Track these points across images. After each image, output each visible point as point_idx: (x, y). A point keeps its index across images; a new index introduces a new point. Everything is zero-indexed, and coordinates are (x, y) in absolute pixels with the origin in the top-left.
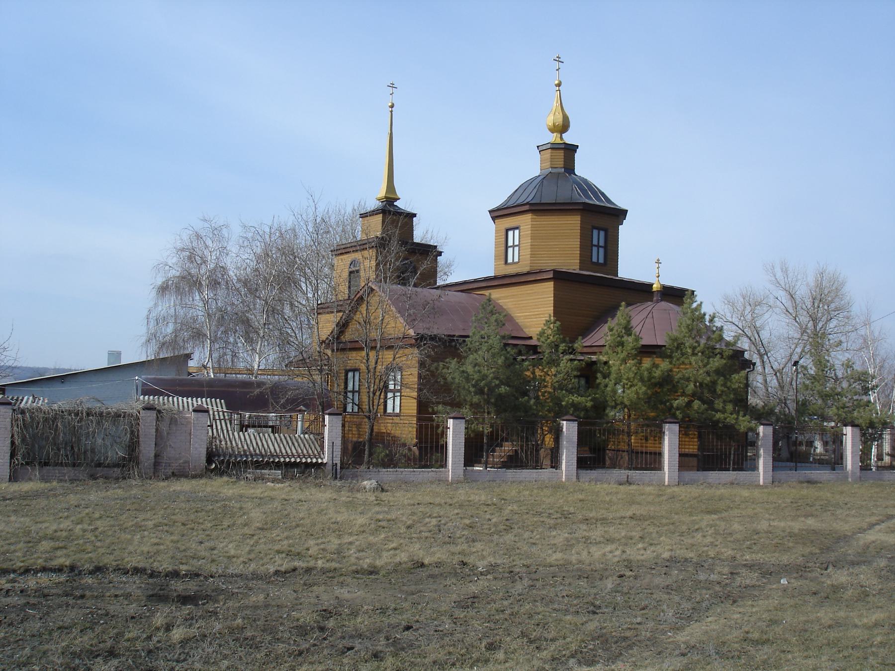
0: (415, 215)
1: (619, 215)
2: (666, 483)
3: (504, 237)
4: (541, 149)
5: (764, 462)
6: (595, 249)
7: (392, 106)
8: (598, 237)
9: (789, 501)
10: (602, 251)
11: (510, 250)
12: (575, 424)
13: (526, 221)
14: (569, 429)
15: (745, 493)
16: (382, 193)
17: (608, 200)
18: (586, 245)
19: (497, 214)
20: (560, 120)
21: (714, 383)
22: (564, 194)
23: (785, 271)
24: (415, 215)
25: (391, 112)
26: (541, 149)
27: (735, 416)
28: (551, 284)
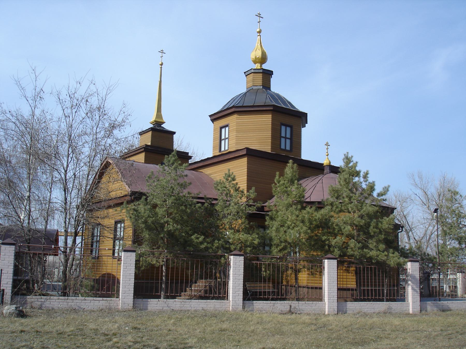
0: (174, 133)
1: (301, 118)
2: (327, 313)
3: (219, 133)
4: (247, 74)
5: (412, 293)
6: (283, 140)
7: (162, 65)
8: (285, 132)
9: (438, 328)
10: (288, 141)
11: (223, 142)
12: (242, 258)
13: (233, 120)
14: (236, 266)
15: (396, 322)
16: (153, 118)
17: (297, 109)
18: (276, 137)
19: (215, 118)
20: (259, 54)
21: (368, 225)
22: (261, 100)
23: (420, 177)
24: (174, 133)
25: (161, 68)
26: (247, 74)
27: (386, 253)
28: (245, 160)
